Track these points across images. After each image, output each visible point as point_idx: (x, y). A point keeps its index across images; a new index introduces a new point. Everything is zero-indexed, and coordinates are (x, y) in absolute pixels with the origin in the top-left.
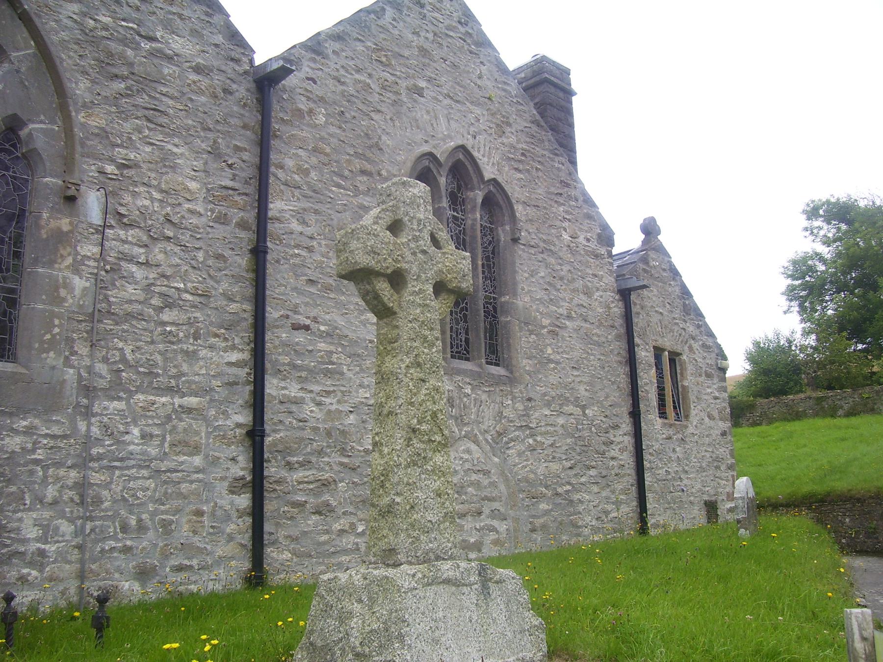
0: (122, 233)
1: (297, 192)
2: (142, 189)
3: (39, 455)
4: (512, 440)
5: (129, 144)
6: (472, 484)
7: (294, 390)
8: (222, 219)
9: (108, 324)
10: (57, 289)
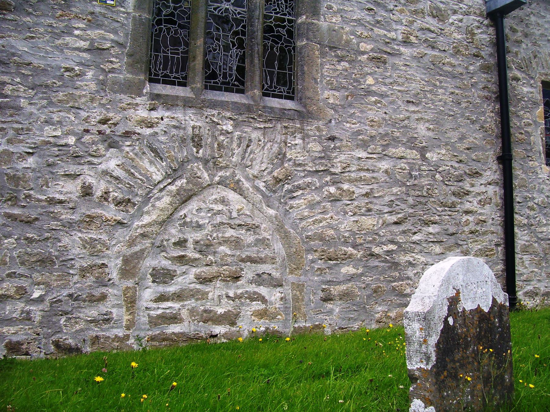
4: (299, 188)
6: (225, 241)
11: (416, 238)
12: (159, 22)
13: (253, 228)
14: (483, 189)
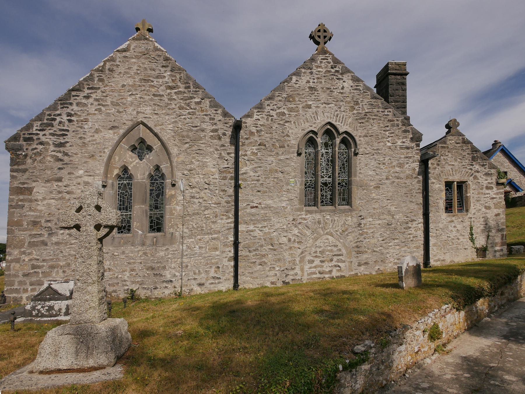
0: (191, 191)
1: (252, 162)
2: (196, 176)
3: (170, 256)
4: (350, 233)
5: (192, 163)
6: (328, 251)
7: (251, 227)
8: (225, 178)
9: (188, 218)
10: (172, 211)
11: (390, 244)
12: (306, 188)
13: (336, 246)
14: (416, 225)
